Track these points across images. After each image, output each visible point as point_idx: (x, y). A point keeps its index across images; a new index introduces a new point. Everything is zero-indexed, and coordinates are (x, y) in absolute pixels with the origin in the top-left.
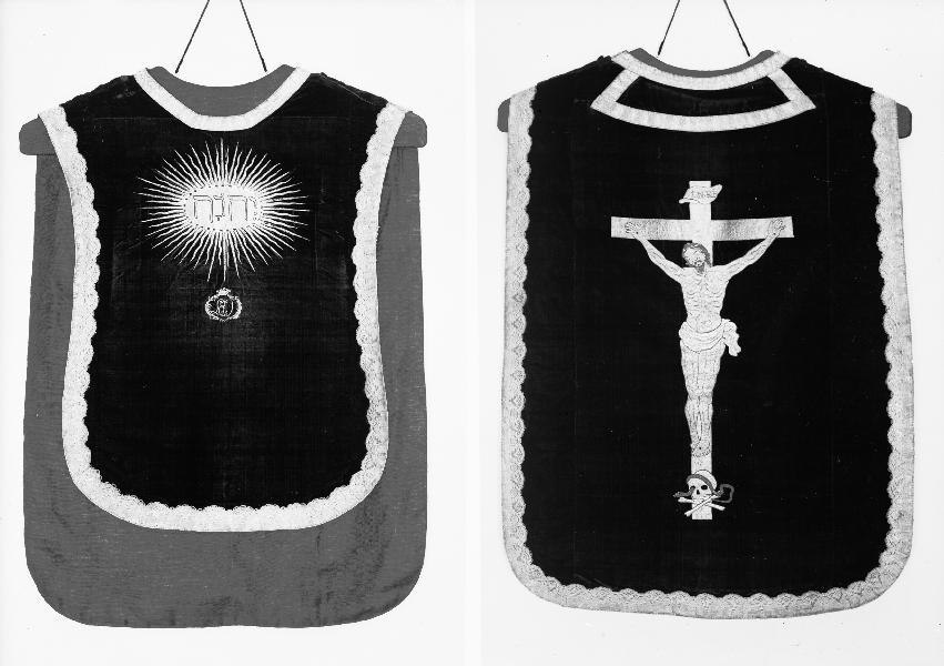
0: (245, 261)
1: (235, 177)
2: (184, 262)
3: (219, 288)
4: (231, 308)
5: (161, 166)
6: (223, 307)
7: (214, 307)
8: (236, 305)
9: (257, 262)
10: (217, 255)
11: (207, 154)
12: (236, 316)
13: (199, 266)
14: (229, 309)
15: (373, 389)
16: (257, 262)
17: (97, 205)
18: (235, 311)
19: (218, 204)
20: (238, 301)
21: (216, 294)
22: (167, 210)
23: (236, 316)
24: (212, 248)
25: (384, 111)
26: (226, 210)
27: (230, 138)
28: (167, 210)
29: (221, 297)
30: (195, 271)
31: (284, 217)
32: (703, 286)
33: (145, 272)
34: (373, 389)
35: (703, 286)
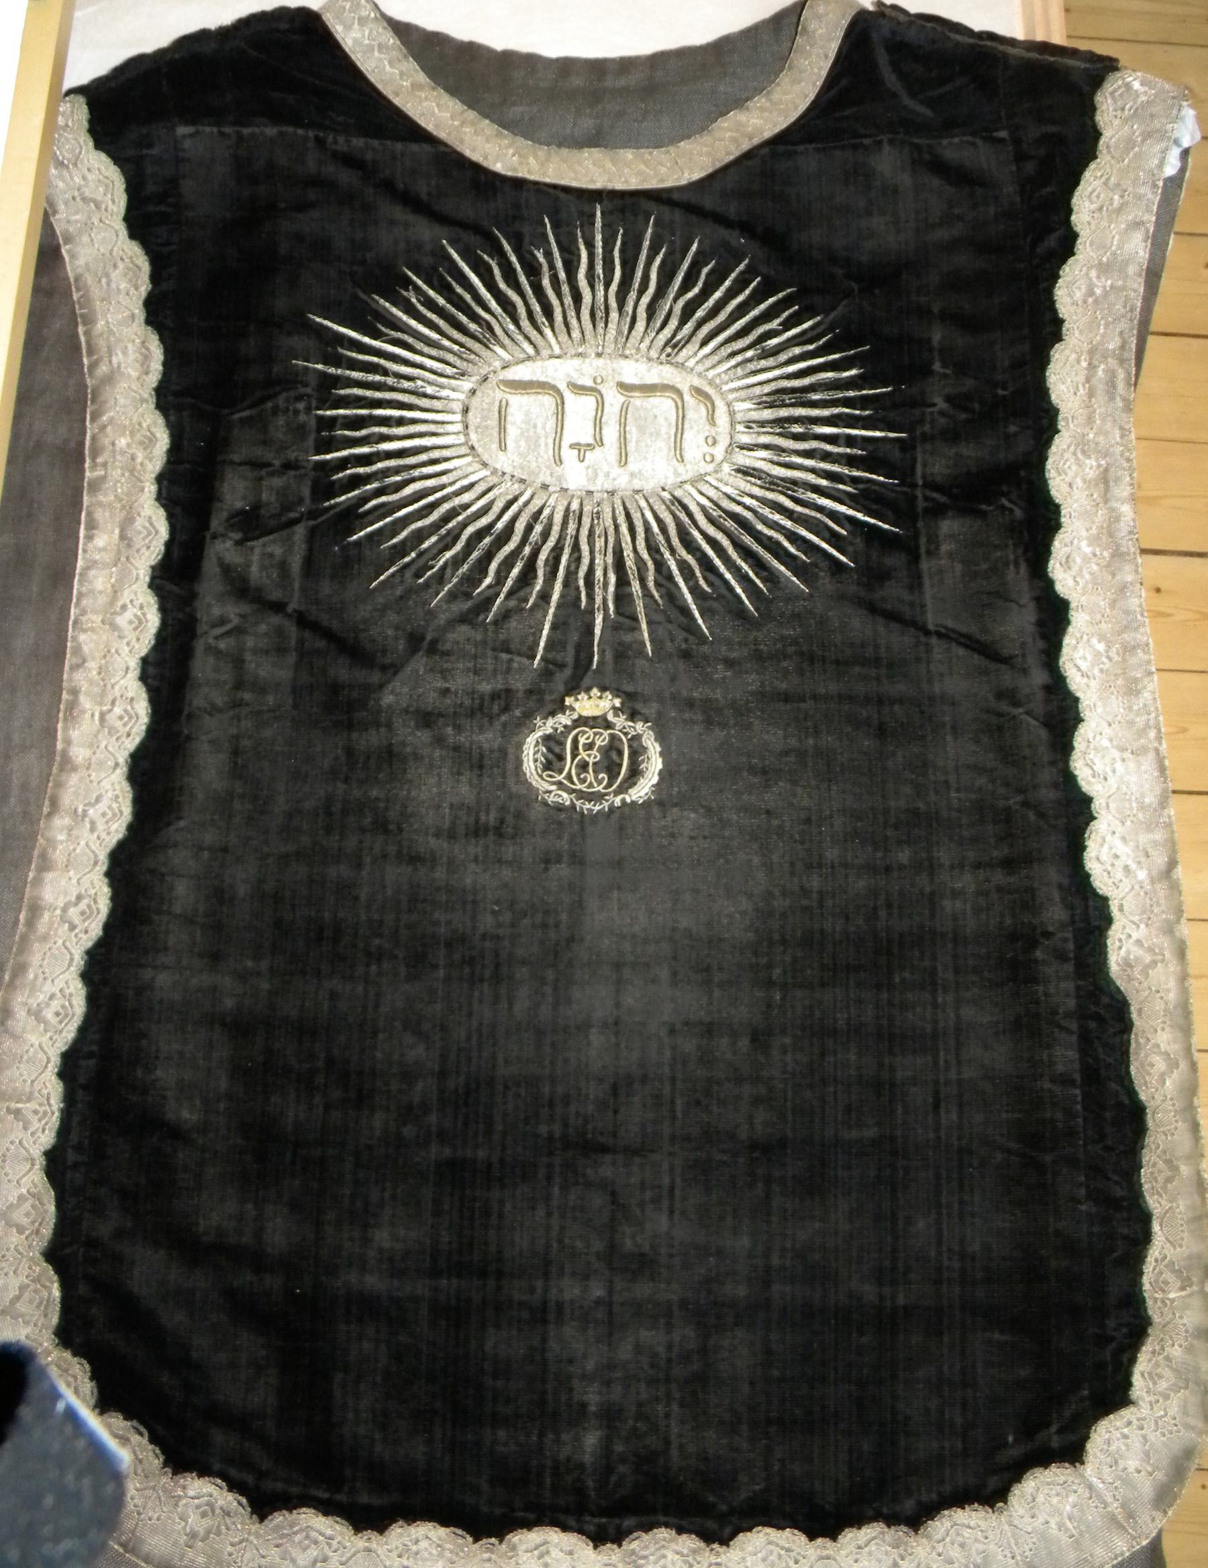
0: (672, 596)
1: (641, 325)
2: (452, 596)
3: (574, 687)
4: (617, 762)
5: (393, 286)
6: (592, 756)
7: (553, 762)
8: (637, 752)
9: (718, 600)
10: (571, 576)
11: (590, 246)
12: (641, 791)
13: (505, 615)
14: (611, 768)
15: (1160, 1064)
16: (718, 600)
17: (167, 398)
18: (635, 773)
19: (580, 409)
20: (653, 748)
21: (561, 708)
22: (401, 422)
23: (641, 791)
24: (557, 551)
25: (1111, 77)
26: (601, 430)
27: (626, 206)
28: (401, 422)
29: (582, 721)
30: (525, 620)
31: (808, 454)
32: (1049, 189)
33: (312, 621)
34: (1160, 1064)
35: (1049, 189)
